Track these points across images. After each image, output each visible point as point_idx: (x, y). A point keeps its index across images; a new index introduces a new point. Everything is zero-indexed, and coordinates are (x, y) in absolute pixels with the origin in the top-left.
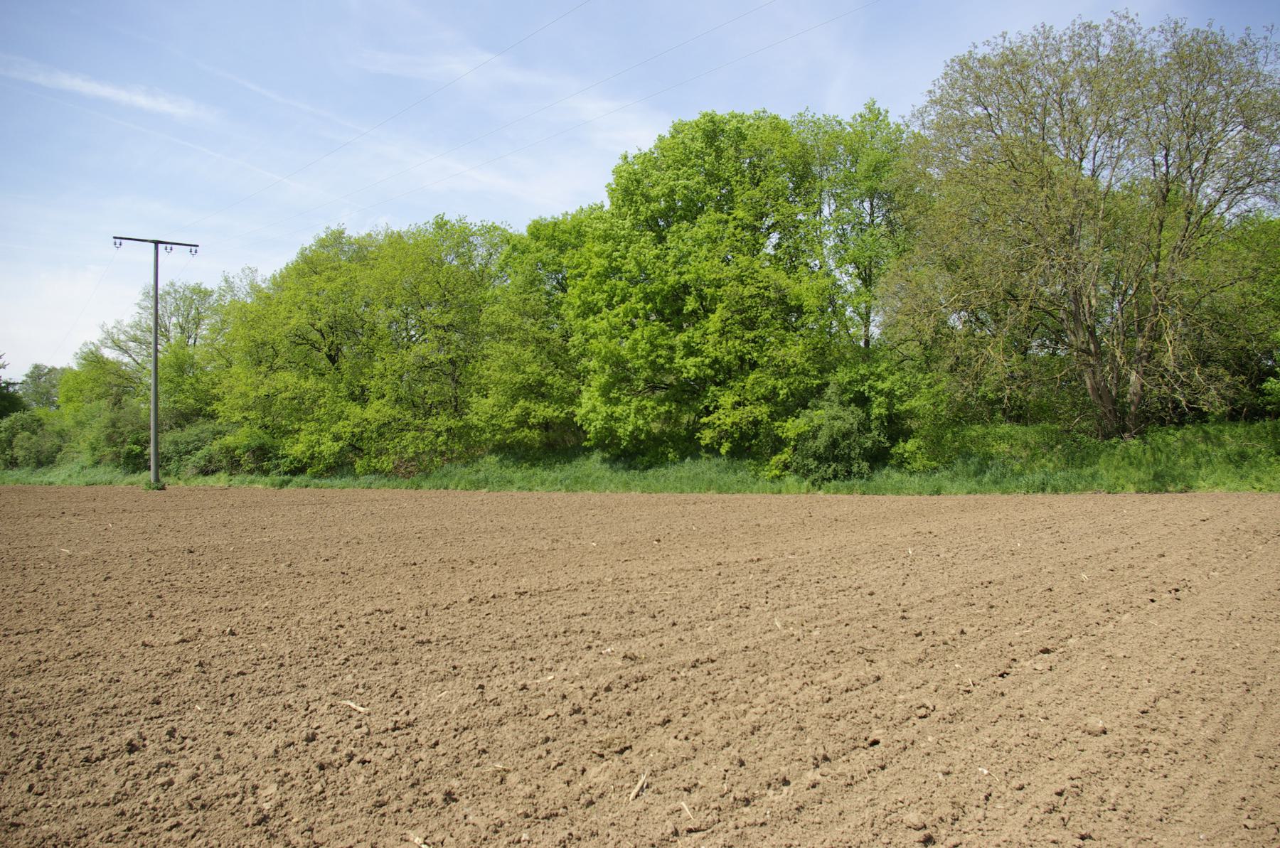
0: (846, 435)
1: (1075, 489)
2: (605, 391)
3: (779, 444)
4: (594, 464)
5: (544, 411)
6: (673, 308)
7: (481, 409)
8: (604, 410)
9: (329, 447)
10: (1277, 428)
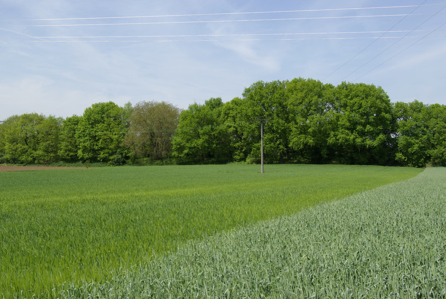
2: (83, 151)
4: (81, 162)
5: (72, 154)
7: (61, 153)
8: (82, 154)
9: (30, 159)
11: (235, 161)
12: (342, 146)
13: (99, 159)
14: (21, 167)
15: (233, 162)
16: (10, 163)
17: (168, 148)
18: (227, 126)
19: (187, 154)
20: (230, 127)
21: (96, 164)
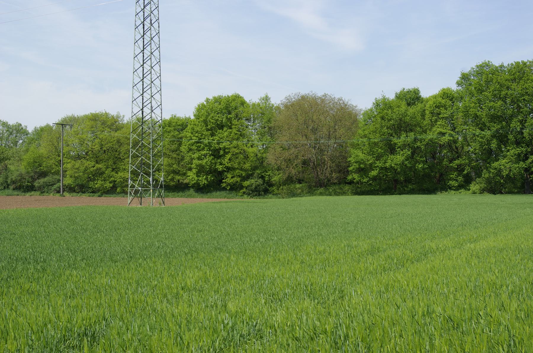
0: (259, 186)
1: (502, 193)
3: (242, 187)
4: (192, 190)
6: (217, 154)
8: (196, 178)
9: (108, 185)
10: (1, 141)
11: (450, 188)
12: (272, 110)
13: (224, 185)
14: (93, 198)
15: (446, 191)
16: (74, 191)
17: (344, 171)
18: (437, 133)
19: (374, 179)
20: (444, 134)
21: (218, 193)
